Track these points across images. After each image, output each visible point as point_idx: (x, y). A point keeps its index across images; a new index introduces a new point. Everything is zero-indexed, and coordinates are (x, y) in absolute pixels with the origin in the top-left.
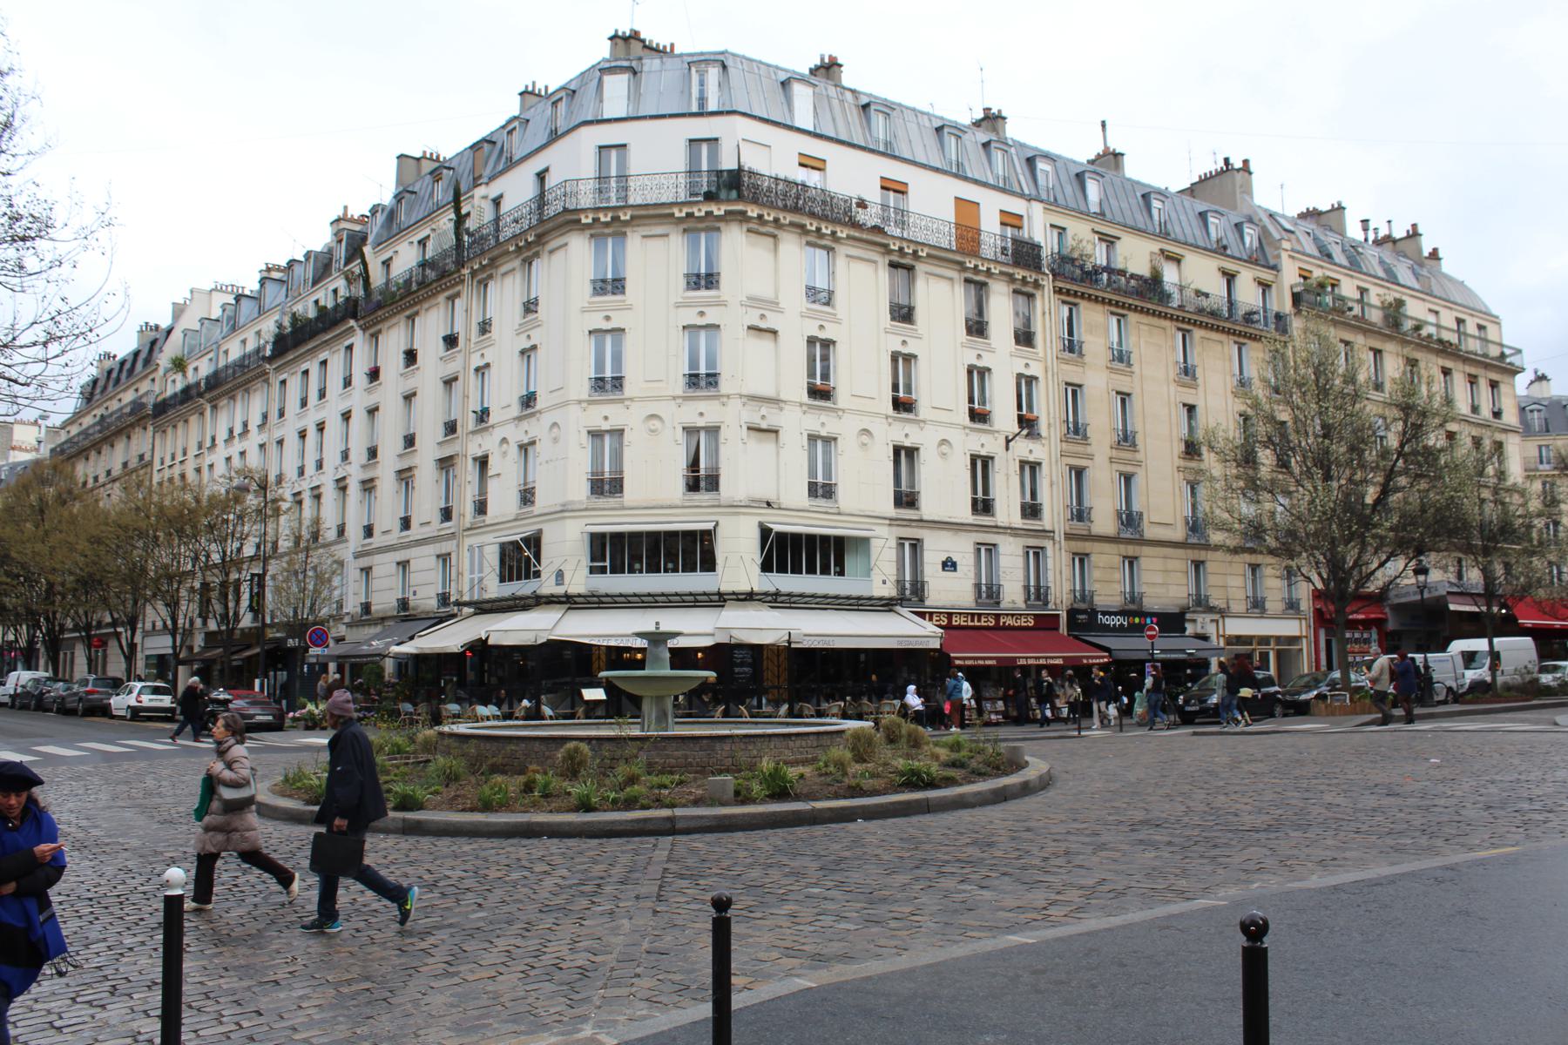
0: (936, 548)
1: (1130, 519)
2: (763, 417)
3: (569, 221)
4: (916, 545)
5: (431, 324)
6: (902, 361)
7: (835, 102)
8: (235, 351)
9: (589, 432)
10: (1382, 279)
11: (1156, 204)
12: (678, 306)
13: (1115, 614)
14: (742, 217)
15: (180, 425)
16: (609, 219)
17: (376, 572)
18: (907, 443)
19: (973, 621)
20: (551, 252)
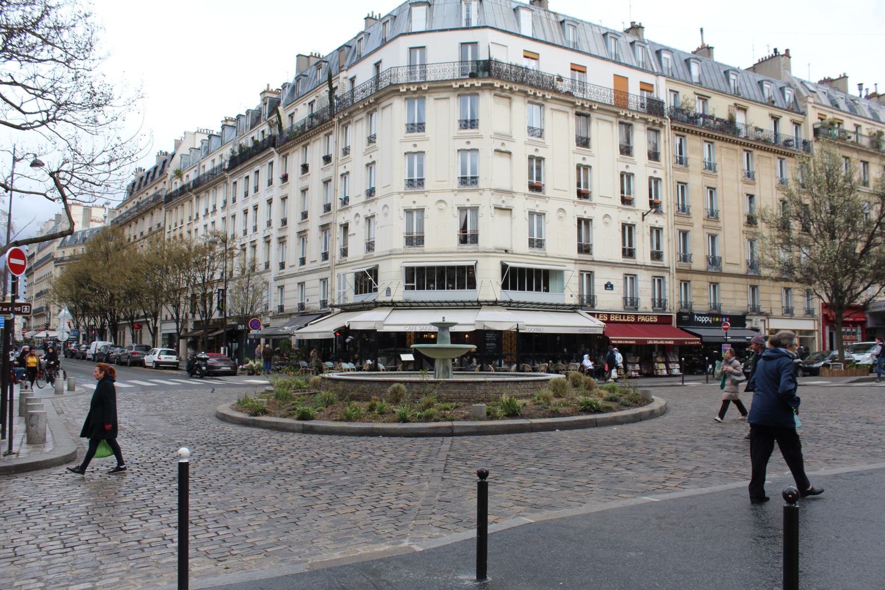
0: (601, 276)
1: (714, 261)
2: (503, 201)
3: (393, 90)
4: (590, 275)
5: (316, 150)
6: (583, 169)
7: (545, 20)
8: (208, 166)
9: (405, 210)
10: (870, 119)
12: (455, 138)
13: (705, 315)
14: (491, 87)
15: (179, 207)
16: (415, 89)
17: (286, 288)
18: (585, 217)
19: (622, 318)
20: (383, 108)
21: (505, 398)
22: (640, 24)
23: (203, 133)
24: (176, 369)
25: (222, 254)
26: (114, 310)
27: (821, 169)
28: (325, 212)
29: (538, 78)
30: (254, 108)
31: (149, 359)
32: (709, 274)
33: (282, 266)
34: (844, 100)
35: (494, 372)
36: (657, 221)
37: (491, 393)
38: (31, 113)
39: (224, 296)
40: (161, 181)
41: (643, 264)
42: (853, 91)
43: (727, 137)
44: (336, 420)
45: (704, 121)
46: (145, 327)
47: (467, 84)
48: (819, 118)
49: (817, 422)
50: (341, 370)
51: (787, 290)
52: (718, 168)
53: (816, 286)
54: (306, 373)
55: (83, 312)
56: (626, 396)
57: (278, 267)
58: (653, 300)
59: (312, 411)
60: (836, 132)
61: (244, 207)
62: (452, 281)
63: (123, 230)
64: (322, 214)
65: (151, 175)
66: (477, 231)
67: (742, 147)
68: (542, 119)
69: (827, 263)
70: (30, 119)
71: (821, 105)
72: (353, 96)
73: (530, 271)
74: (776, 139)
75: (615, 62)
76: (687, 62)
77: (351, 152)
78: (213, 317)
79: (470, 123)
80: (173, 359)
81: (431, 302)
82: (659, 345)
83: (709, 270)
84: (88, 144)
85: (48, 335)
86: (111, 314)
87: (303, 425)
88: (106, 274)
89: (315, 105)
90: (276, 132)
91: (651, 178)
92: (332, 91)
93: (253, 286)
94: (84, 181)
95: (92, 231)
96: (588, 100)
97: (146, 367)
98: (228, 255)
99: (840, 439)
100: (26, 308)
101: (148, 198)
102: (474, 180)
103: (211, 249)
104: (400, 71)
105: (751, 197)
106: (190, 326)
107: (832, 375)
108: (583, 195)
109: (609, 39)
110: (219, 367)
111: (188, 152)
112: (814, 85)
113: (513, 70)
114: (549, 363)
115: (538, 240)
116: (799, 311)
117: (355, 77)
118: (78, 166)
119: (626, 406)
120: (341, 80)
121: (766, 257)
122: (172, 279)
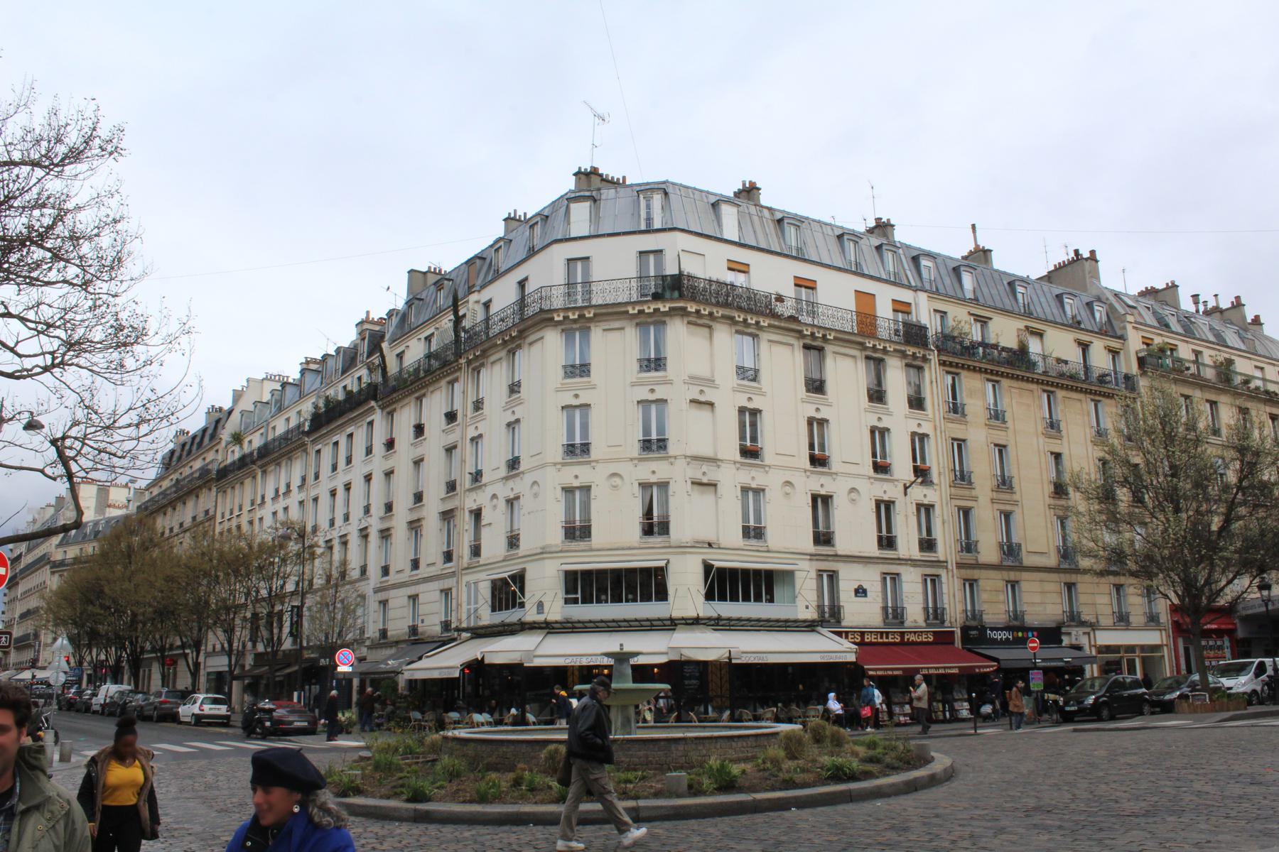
0: (849, 577)
1: (1010, 550)
2: (704, 473)
3: (545, 319)
4: (833, 576)
5: (435, 404)
6: (817, 425)
7: (756, 219)
8: (280, 427)
9: (563, 488)
10: (1213, 343)
11: (1020, 289)
12: (633, 385)
13: (1002, 629)
14: (683, 312)
15: (237, 486)
16: (576, 317)
17: (391, 604)
18: (823, 492)
19: (882, 638)
20: (531, 344)
21: (714, 762)
22: (888, 220)
23: (274, 381)
24: (226, 725)
25: (298, 555)
26: (137, 638)
27: (1153, 414)
28: (448, 493)
29: (749, 298)
30: (346, 345)
31: (186, 711)
32: (1003, 569)
33: (386, 571)
34: (1175, 318)
35: (697, 724)
36: (925, 496)
37: (694, 756)
38: (29, 356)
39: (300, 616)
40: (211, 448)
41: (907, 557)
42: (1187, 305)
43: (1018, 373)
44: (464, 802)
45: (984, 352)
46: (181, 663)
47: (651, 308)
48: (1143, 343)
49: (1178, 784)
50: (472, 725)
51: (1118, 587)
52: (1008, 416)
53: (1158, 581)
54: (419, 729)
55: (90, 641)
56: (893, 754)
57: (380, 572)
58: (926, 609)
59: (425, 785)
60: (1168, 361)
61: (331, 486)
62: (631, 589)
63: (154, 519)
64: (443, 495)
65: (198, 440)
66: (668, 516)
67: (1040, 386)
68: (757, 356)
69: (1173, 547)
70: (28, 363)
71: (1146, 325)
72: (487, 328)
73: (746, 572)
74: (1086, 374)
75: (855, 273)
76: (956, 271)
77: (485, 406)
78: (283, 648)
79: (655, 363)
80: (222, 710)
81: (602, 621)
82: (937, 675)
83: (1004, 563)
84: (109, 398)
85: (34, 677)
86: (131, 643)
87: (415, 810)
88: (126, 585)
89: (434, 341)
90: (378, 378)
91: (914, 434)
92: (458, 320)
93: (342, 601)
94: (100, 452)
95: (108, 521)
96: (821, 327)
97: (181, 723)
98: (307, 556)
99: (1214, 809)
100: (4, 639)
101: (192, 474)
102: (662, 444)
103: (281, 547)
104: (553, 292)
105: (1057, 456)
106: (249, 661)
107: (1194, 710)
108: (818, 461)
109: (846, 243)
110: (292, 723)
111: (251, 408)
112: (1133, 298)
113: (713, 287)
114: (777, 707)
115: (756, 528)
116: (1137, 618)
117: (490, 301)
118: (93, 429)
119: (893, 769)
120: (471, 305)
121: (1084, 541)
122: (223, 591)
